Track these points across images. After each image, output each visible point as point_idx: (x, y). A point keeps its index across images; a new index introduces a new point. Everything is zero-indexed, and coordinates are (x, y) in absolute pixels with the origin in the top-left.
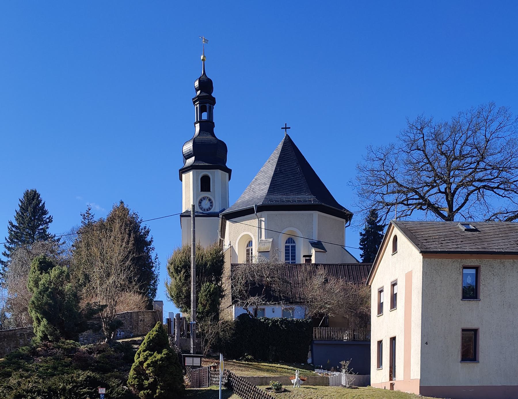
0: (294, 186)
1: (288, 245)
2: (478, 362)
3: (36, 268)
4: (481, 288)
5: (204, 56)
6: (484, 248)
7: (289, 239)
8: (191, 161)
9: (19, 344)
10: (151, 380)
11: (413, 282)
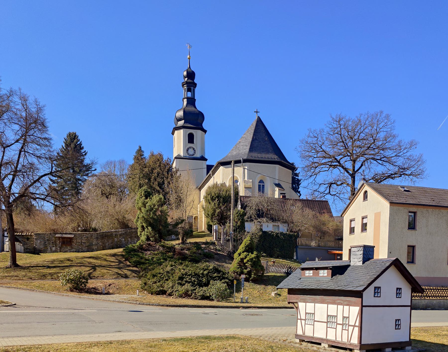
0: (264, 149)
1: (260, 184)
2: (415, 264)
3: (142, 195)
4: (417, 223)
5: (190, 56)
6: (419, 202)
7: (261, 180)
8: (181, 123)
9: (114, 241)
10: (249, 269)
11: (381, 218)
